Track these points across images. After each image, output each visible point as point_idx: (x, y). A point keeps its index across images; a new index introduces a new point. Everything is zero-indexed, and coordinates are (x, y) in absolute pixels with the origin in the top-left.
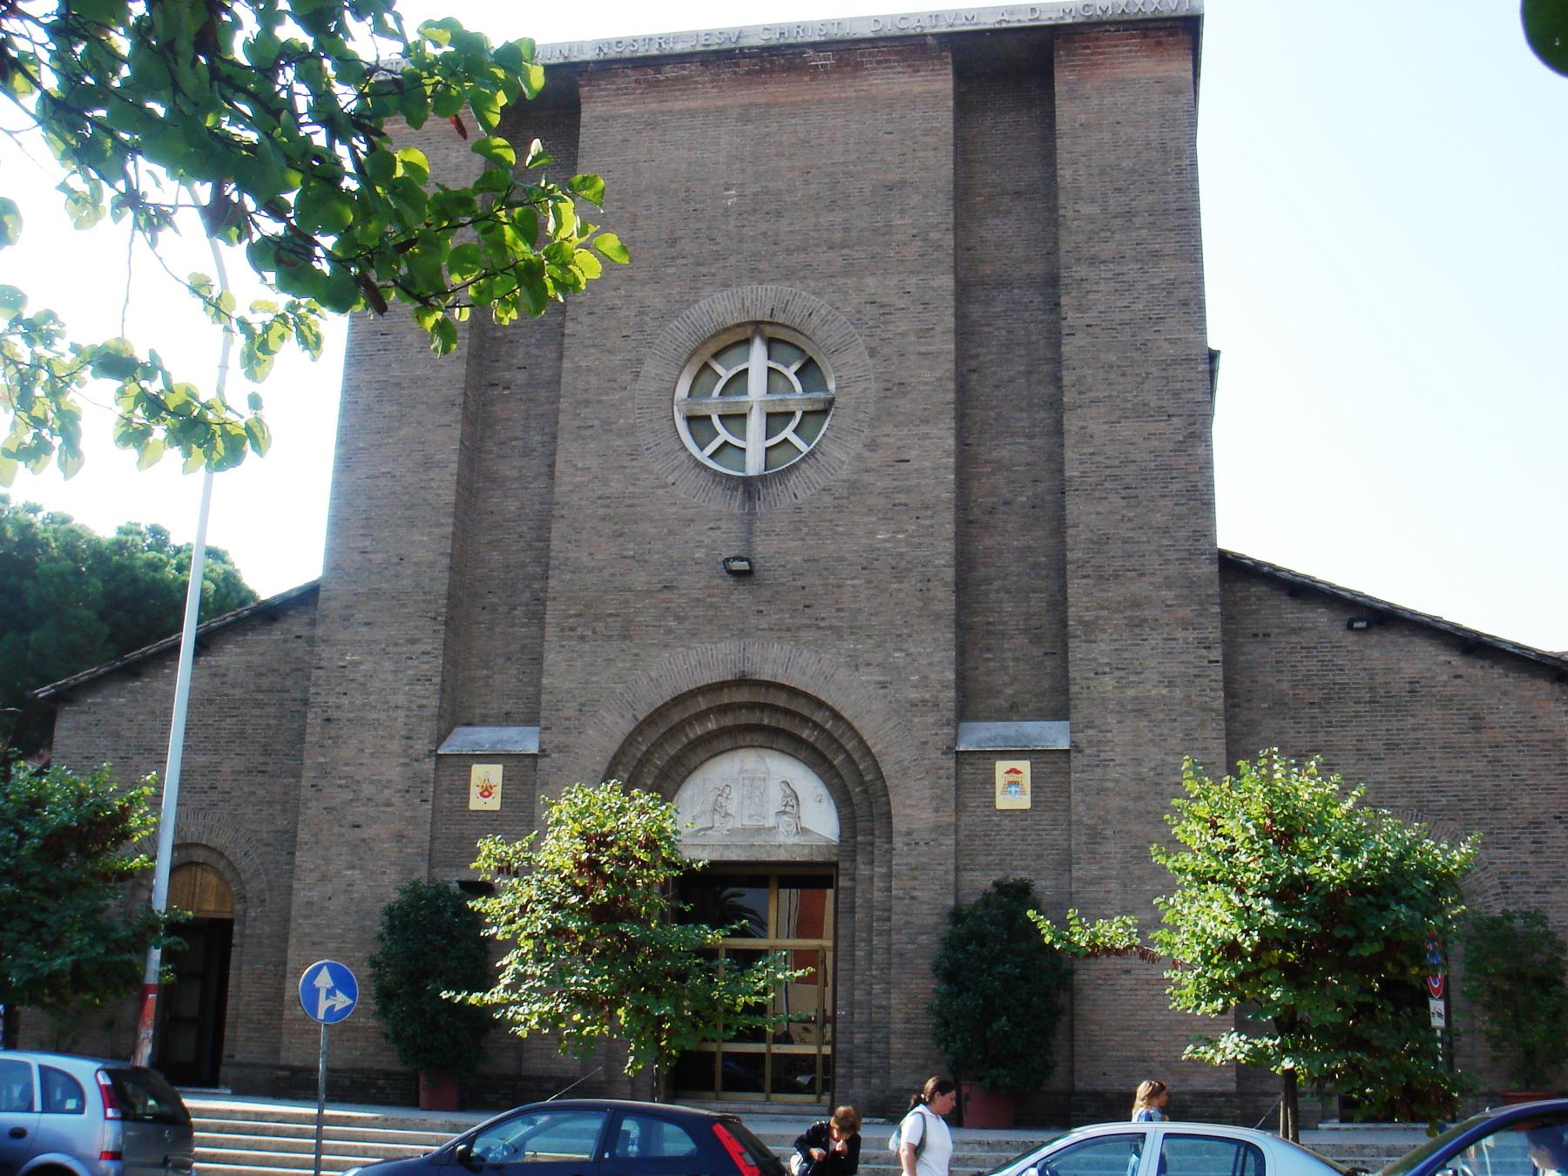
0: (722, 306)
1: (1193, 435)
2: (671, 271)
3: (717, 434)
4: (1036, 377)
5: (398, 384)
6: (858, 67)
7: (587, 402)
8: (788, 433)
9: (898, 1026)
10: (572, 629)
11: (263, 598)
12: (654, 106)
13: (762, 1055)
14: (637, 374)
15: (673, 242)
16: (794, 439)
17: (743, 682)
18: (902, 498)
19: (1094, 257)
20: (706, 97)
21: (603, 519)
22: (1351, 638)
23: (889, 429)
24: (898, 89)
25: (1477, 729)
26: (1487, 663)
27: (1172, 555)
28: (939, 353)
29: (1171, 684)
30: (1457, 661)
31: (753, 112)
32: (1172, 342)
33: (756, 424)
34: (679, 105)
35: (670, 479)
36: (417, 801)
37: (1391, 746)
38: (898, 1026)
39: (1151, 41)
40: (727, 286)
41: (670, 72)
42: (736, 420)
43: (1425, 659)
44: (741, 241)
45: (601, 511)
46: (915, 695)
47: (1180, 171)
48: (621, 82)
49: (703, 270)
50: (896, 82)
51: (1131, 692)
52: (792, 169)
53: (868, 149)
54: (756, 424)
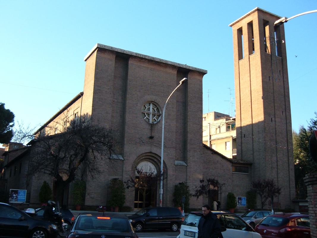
0: (149, 98)
1: (201, 128)
2: (142, 91)
3: (146, 116)
4: (181, 115)
5: (102, 99)
6: (166, 67)
7: (130, 108)
8: (147, 116)
9: (168, 200)
10: (128, 142)
11: (212, 148)
12: (139, 64)
13: (139, 201)
14: (137, 105)
15: (142, 86)
16: (145, 118)
17: (151, 153)
18: (170, 130)
19: (191, 102)
20: (146, 65)
21: (133, 126)
22: (212, 155)
23: (168, 120)
24: (170, 72)
25: (223, 167)
26: (224, 159)
27: (198, 143)
28: (174, 111)
29: (198, 159)
30: (221, 159)
31: (152, 69)
32: (199, 115)
33: (151, 116)
34: (143, 65)
35: (142, 122)
36: (106, 165)
37: (215, 168)
38: (168, 200)
39: (200, 74)
40: (149, 95)
41: (143, 60)
42: (149, 115)
43: (219, 158)
44: (151, 89)
45: (132, 125)
46: (171, 157)
47: (96, 77)
48: (136, 59)
49: (146, 92)
50: (170, 70)
51: (194, 159)
52: (157, 79)
53: (167, 79)
54: (151, 116)
